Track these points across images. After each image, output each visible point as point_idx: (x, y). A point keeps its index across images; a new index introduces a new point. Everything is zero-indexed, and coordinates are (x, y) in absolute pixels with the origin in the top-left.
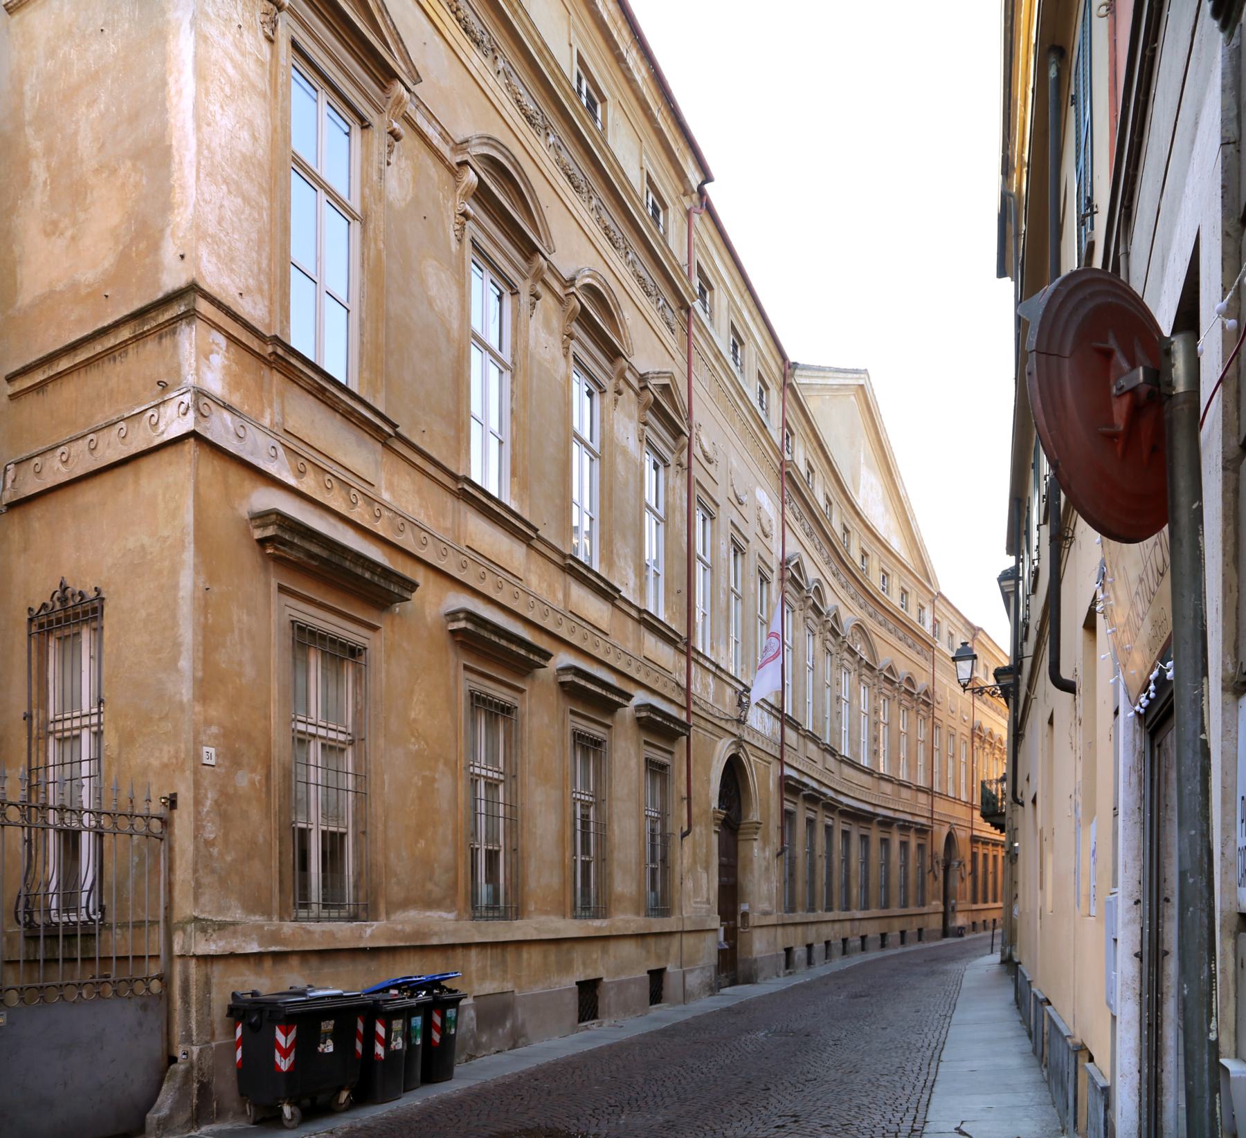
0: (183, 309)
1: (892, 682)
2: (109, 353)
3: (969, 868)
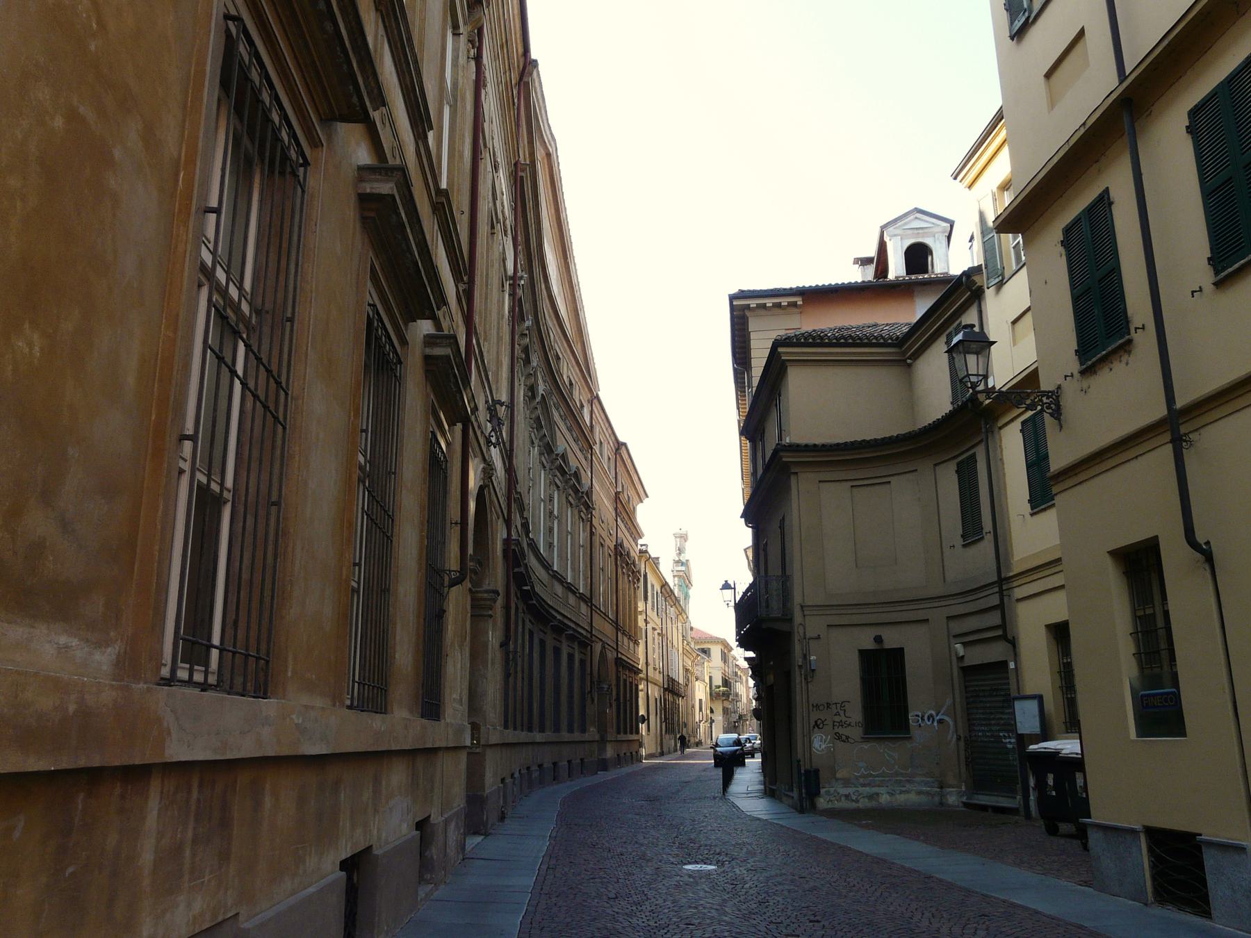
3: (614, 693)
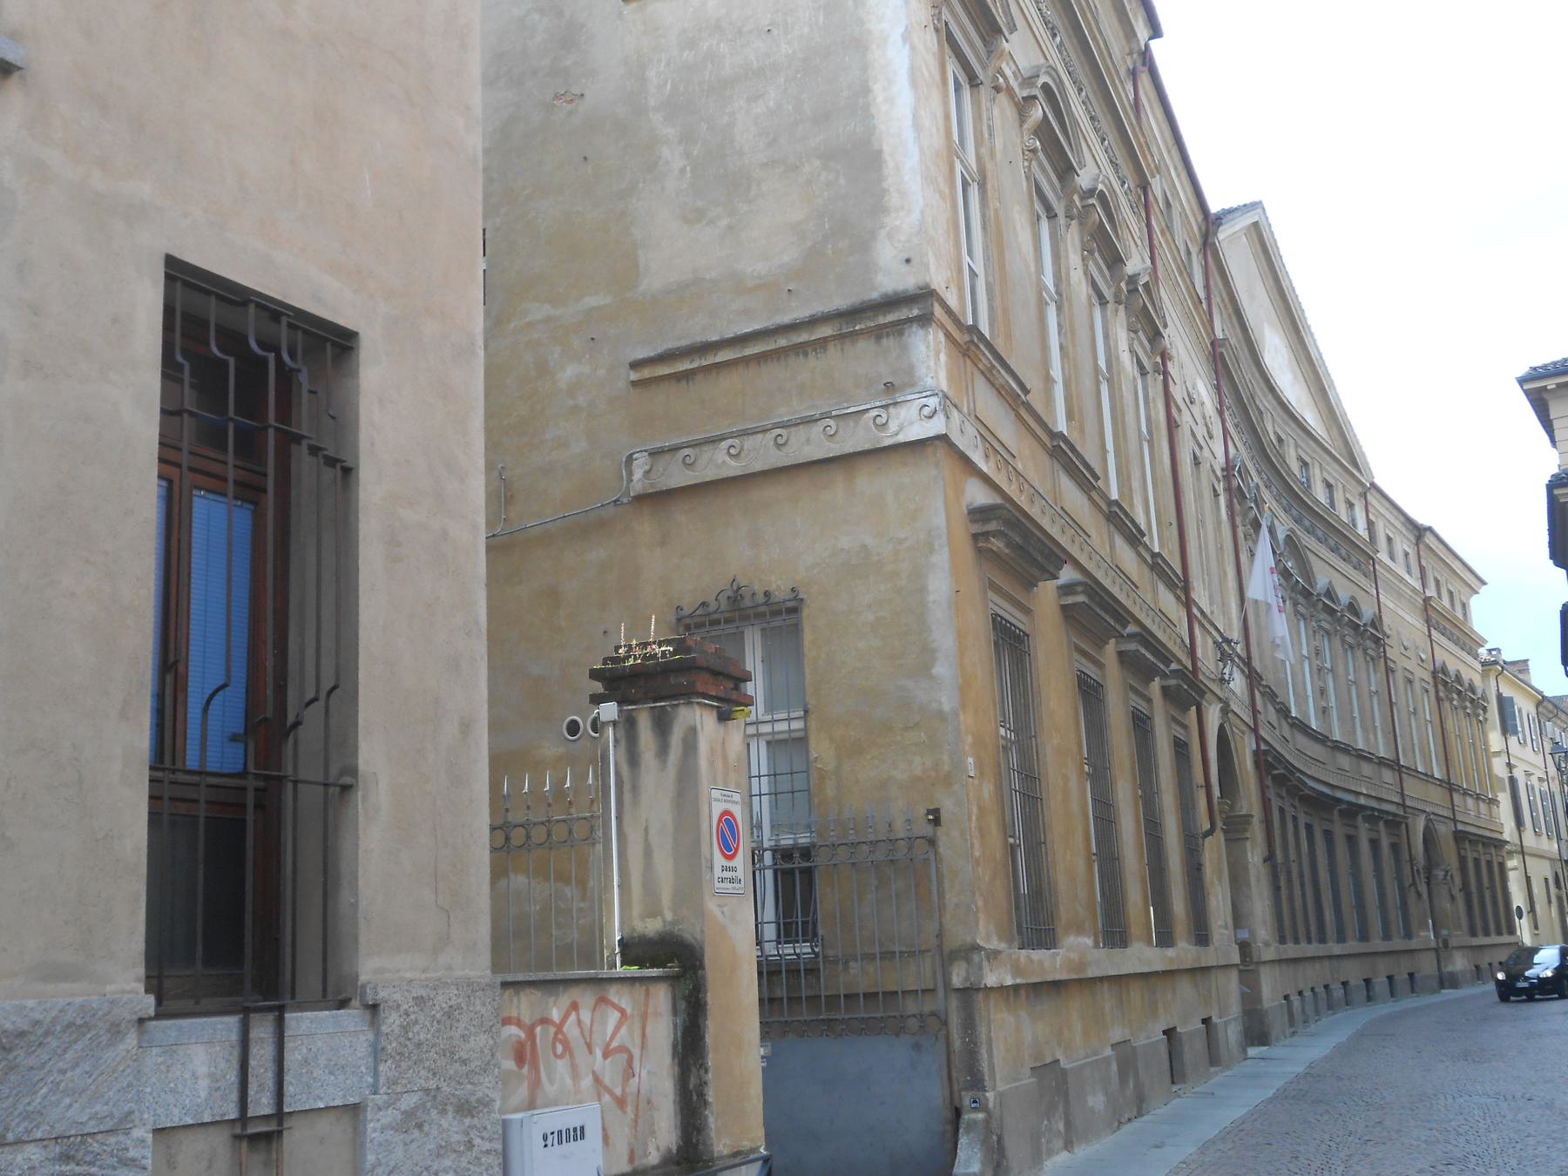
0: (915, 312)
1: (1332, 612)
2: (801, 349)
3: (1458, 880)
